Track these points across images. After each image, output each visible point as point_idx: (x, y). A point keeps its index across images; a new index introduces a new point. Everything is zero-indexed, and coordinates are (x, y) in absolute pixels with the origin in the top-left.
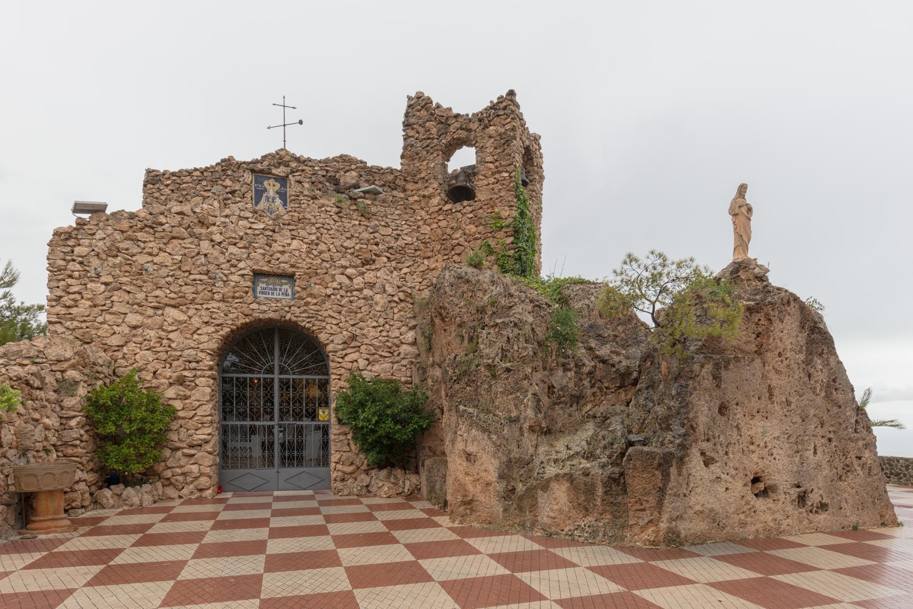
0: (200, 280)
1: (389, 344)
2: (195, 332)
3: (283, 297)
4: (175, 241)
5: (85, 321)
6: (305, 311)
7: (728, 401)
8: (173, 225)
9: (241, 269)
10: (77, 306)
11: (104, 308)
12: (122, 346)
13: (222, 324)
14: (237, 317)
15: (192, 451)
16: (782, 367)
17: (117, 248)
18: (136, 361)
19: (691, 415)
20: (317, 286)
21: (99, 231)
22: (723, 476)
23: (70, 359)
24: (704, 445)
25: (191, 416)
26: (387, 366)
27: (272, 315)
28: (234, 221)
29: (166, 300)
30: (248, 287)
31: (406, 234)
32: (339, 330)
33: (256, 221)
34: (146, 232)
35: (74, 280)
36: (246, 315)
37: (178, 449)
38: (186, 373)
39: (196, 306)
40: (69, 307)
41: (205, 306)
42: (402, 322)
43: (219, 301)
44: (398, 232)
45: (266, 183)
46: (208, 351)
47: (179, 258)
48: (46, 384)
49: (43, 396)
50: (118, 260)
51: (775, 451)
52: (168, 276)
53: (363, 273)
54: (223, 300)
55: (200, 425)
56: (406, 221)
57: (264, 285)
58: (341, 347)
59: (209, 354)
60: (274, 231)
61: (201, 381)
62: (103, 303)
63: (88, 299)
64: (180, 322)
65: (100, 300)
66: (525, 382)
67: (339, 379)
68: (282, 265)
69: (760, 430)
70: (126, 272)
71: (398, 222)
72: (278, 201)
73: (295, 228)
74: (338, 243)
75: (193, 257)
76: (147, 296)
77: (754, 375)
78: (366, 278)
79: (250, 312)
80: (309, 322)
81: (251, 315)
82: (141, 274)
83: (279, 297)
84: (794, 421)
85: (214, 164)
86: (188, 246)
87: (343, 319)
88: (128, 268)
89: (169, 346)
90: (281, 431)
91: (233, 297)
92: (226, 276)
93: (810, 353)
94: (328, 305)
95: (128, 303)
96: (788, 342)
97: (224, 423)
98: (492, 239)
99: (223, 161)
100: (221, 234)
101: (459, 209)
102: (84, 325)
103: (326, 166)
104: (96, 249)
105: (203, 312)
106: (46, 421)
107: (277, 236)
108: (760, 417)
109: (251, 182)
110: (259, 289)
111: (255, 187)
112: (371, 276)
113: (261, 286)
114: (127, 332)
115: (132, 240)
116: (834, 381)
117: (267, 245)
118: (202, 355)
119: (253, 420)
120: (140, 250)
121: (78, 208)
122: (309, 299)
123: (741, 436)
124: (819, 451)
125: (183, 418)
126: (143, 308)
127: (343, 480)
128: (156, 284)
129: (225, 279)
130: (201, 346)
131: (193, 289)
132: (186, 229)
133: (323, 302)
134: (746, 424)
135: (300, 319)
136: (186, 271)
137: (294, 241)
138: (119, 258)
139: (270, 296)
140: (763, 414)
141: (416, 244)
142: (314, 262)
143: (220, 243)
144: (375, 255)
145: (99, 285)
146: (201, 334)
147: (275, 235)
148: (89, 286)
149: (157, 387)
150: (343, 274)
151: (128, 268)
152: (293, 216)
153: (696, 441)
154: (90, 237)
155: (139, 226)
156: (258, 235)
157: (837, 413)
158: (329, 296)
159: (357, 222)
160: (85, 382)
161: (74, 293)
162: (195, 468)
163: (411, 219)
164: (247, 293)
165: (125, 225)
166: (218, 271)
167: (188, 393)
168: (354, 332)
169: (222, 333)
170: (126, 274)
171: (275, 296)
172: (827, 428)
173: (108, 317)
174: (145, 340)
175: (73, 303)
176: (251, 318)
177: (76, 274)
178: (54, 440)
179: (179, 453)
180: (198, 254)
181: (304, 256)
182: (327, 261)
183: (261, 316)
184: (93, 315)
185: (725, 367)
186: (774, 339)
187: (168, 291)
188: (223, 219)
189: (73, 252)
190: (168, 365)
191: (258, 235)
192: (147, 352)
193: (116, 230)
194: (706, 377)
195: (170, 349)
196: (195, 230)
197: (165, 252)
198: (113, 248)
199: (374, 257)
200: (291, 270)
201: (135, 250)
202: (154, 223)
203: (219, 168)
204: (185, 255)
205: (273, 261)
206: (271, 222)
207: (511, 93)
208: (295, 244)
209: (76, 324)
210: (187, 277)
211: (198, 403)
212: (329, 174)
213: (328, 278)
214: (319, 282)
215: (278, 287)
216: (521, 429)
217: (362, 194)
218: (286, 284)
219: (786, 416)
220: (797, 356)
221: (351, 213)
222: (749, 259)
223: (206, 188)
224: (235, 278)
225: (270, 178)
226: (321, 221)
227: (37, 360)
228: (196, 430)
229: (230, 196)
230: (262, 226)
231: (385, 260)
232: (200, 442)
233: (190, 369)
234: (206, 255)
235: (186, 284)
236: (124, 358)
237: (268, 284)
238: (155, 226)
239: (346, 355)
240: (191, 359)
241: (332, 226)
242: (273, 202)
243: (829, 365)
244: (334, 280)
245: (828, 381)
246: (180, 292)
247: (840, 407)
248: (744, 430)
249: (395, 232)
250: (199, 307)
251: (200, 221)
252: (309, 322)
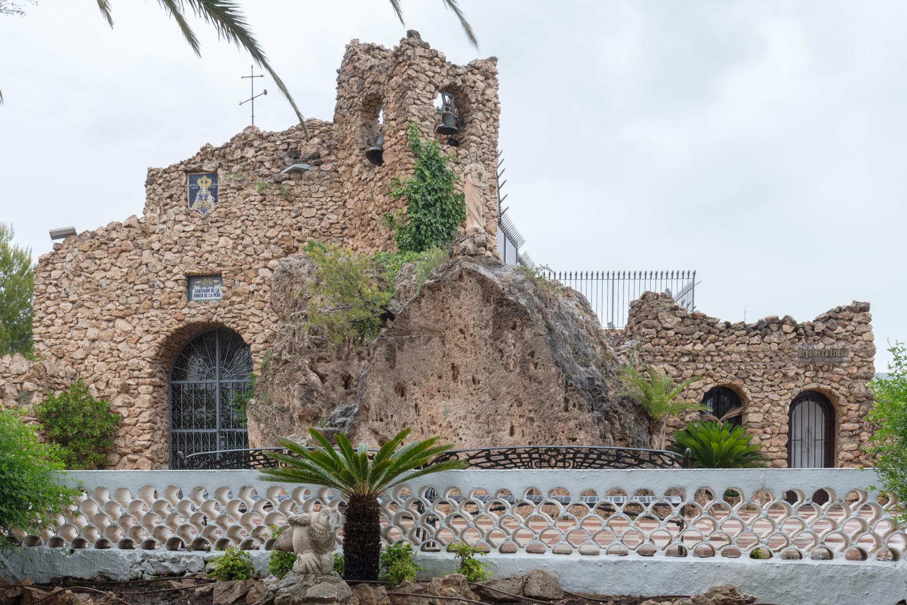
0: (143, 290)
2: (138, 341)
4: (124, 255)
5: (58, 338)
6: (230, 311)
7: (404, 381)
10: (53, 325)
11: (72, 325)
12: (84, 359)
14: (171, 324)
15: (135, 457)
16: (466, 344)
17: (81, 268)
19: (364, 396)
20: (241, 284)
21: (69, 254)
23: (25, 373)
24: (376, 425)
25: (134, 422)
29: (116, 313)
30: (181, 292)
31: (332, 212)
32: (261, 328)
33: (188, 223)
34: (102, 249)
35: (51, 302)
36: (180, 321)
37: (125, 454)
38: (131, 382)
39: (139, 316)
40: (48, 326)
41: (145, 315)
43: (157, 309)
44: (323, 211)
45: (199, 181)
46: (148, 359)
47: (125, 270)
48: (7, 394)
50: (80, 280)
51: (460, 432)
52: (118, 289)
54: (161, 308)
55: (141, 432)
56: (332, 197)
58: (262, 346)
59: (149, 362)
60: (203, 231)
61: (142, 389)
62: (71, 320)
63: (61, 318)
64: (126, 332)
65: (69, 318)
66: (299, 373)
68: (211, 265)
69: (441, 410)
70: (87, 289)
71: (323, 200)
72: (210, 198)
73: (223, 224)
74: (261, 234)
75: (137, 268)
76: (102, 310)
77: (432, 354)
79: (183, 317)
80: (233, 323)
81: (183, 320)
82: (97, 290)
84: (482, 399)
86: (133, 257)
87: (265, 316)
88: (88, 285)
89: (119, 357)
90: (223, 439)
91: (169, 304)
93: (498, 327)
94: (251, 303)
95: (88, 318)
96: (469, 318)
97: (174, 431)
100: (159, 241)
102: (58, 342)
103: (288, 138)
104: (66, 271)
105: (144, 321)
107: (206, 236)
108: (442, 396)
109: (186, 183)
110: (194, 292)
111: (190, 188)
113: (196, 288)
114: (87, 345)
115: (91, 258)
116: (532, 354)
118: (143, 363)
119: (197, 428)
120: (96, 267)
121: (54, 236)
122: (234, 298)
124: (517, 431)
125: (129, 425)
126: (99, 322)
128: (108, 298)
129: (162, 286)
131: (136, 299)
132: (132, 241)
133: (247, 299)
134: (425, 403)
135: (225, 320)
136: (131, 283)
137: (222, 238)
138: (82, 277)
140: (444, 393)
141: (343, 222)
142: (239, 258)
143: (158, 250)
144: (299, 241)
145: (68, 304)
147: (204, 235)
148: (61, 306)
149: (109, 396)
150: (265, 267)
151: (88, 285)
152: (220, 212)
153: (366, 421)
154: (62, 260)
155: (97, 244)
156: (190, 237)
157: (538, 390)
158: (253, 292)
159: (279, 208)
161: (51, 313)
163: (336, 194)
164: (180, 298)
165: (87, 243)
166: (156, 279)
167: (133, 401)
168: (275, 330)
169: (159, 340)
170: (87, 291)
172: (526, 406)
173: (75, 333)
174: (101, 352)
175: (50, 322)
176: (183, 322)
177: (52, 296)
179: (125, 458)
180: (141, 264)
181: (229, 252)
182: (251, 255)
183: (192, 320)
184: (64, 332)
185: (399, 348)
186: (451, 316)
187: (118, 304)
188: (162, 226)
190: (117, 375)
191: (190, 237)
192: (102, 363)
193: (80, 251)
194: (379, 359)
195: (118, 359)
196: (138, 241)
197: (116, 266)
198: (78, 269)
199: (296, 244)
201: (93, 268)
202: (108, 239)
205: (203, 262)
206: (200, 223)
208: (222, 241)
209: (53, 341)
210: (132, 288)
211: (139, 410)
212: (290, 147)
213: (251, 274)
214: (243, 278)
215: (210, 288)
216: (291, 418)
217: (287, 175)
219: (472, 394)
220: (483, 332)
221: (275, 198)
224: (170, 284)
225: (203, 175)
226: (244, 213)
228: (139, 436)
229: (169, 200)
230: (192, 227)
232: (140, 447)
233: (134, 377)
234: (146, 265)
236: (86, 370)
237: (202, 286)
238: (108, 242)
240: (134, 368)
241: (257, 217)
242: (206, 200)
243: (523, 338)
245: (522, 356)
246: (127, 303)
247: (540, 383)
248: (422, 410)
249: (319, 212)
250: (141, 316)
251: (143, 232)
252: (233, 323)
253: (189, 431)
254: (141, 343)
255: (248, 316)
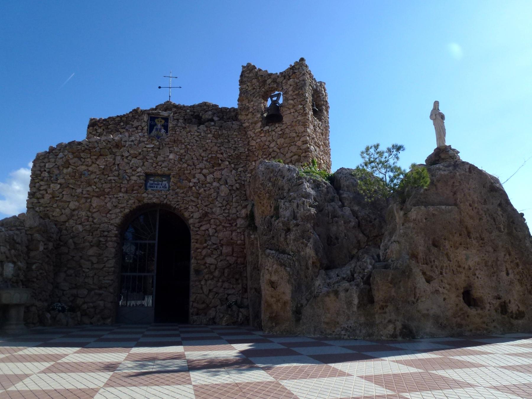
1: (230, 218)
3: (163, 189)
8: (101, 147)
9: (138, 172)
11: (58, 199)
13: (124, 207)
15: (101, 292)
18: (73, 232)
22: (441, 290)
26: (227, 233)
27: (155, 200)
28: (136, 144)
31: (241, 147)
39: (110, 196)
42: (238, 203)
46: (115, 225)
49: (20, 248)
51: (477, 273)
53: (213, 172)
54: (126, 192)
55: (107, 274)
57: (152, 182)
63: (50, 194)
67: (196, 243)
68: (164, 169)
71: (236, 139)
72: (163, 131)
78: (215, 175)
83: (160, 189)
85: (128, 112)
92: (129, 177)
98: (294, 146)
99: (134, 110)
101: (273, 129)
105: (114, 200)
106: (19, 264)
109: (148, 121)
110: (148, 184)
111: (150, 123)
112: (219, 173)
117: (155, 157)
118: (111, 227)
123: (450, 261)
127: (197, 314)
130: (112, 222)
132: (108, 150)
138: (70, 169)
139: (155, 189)
143: (127, 157)
146: (112, 214)
150: (200, 173)
160: (43, 242)
162: (101, 303)
164: (140, 187)
168: (206, 210)
171: (158, 189)
173: (60, 204)
178: (22, 277)
187: (95, 187)
188: (130, 143)
189: (45, 166)
200: (169, 172)
203: (131, 115)
204: (107, 165)
207: (302, 60)
208: (171, 156)
212: (195, 114)
215: (160, 183)
218: (165, 181)
222: (446, 147)
223: (123, 127)
224: (134, 178)
227: (19, 228)
231: (227, 163)
233: (104, 236)
235: (105, 183)
239: (201, 226)
240: (104, 229)
244: (194, 177)
248: (452, 256)
253: (134, 274)
254: (110, 214)
255: (188, 201)
